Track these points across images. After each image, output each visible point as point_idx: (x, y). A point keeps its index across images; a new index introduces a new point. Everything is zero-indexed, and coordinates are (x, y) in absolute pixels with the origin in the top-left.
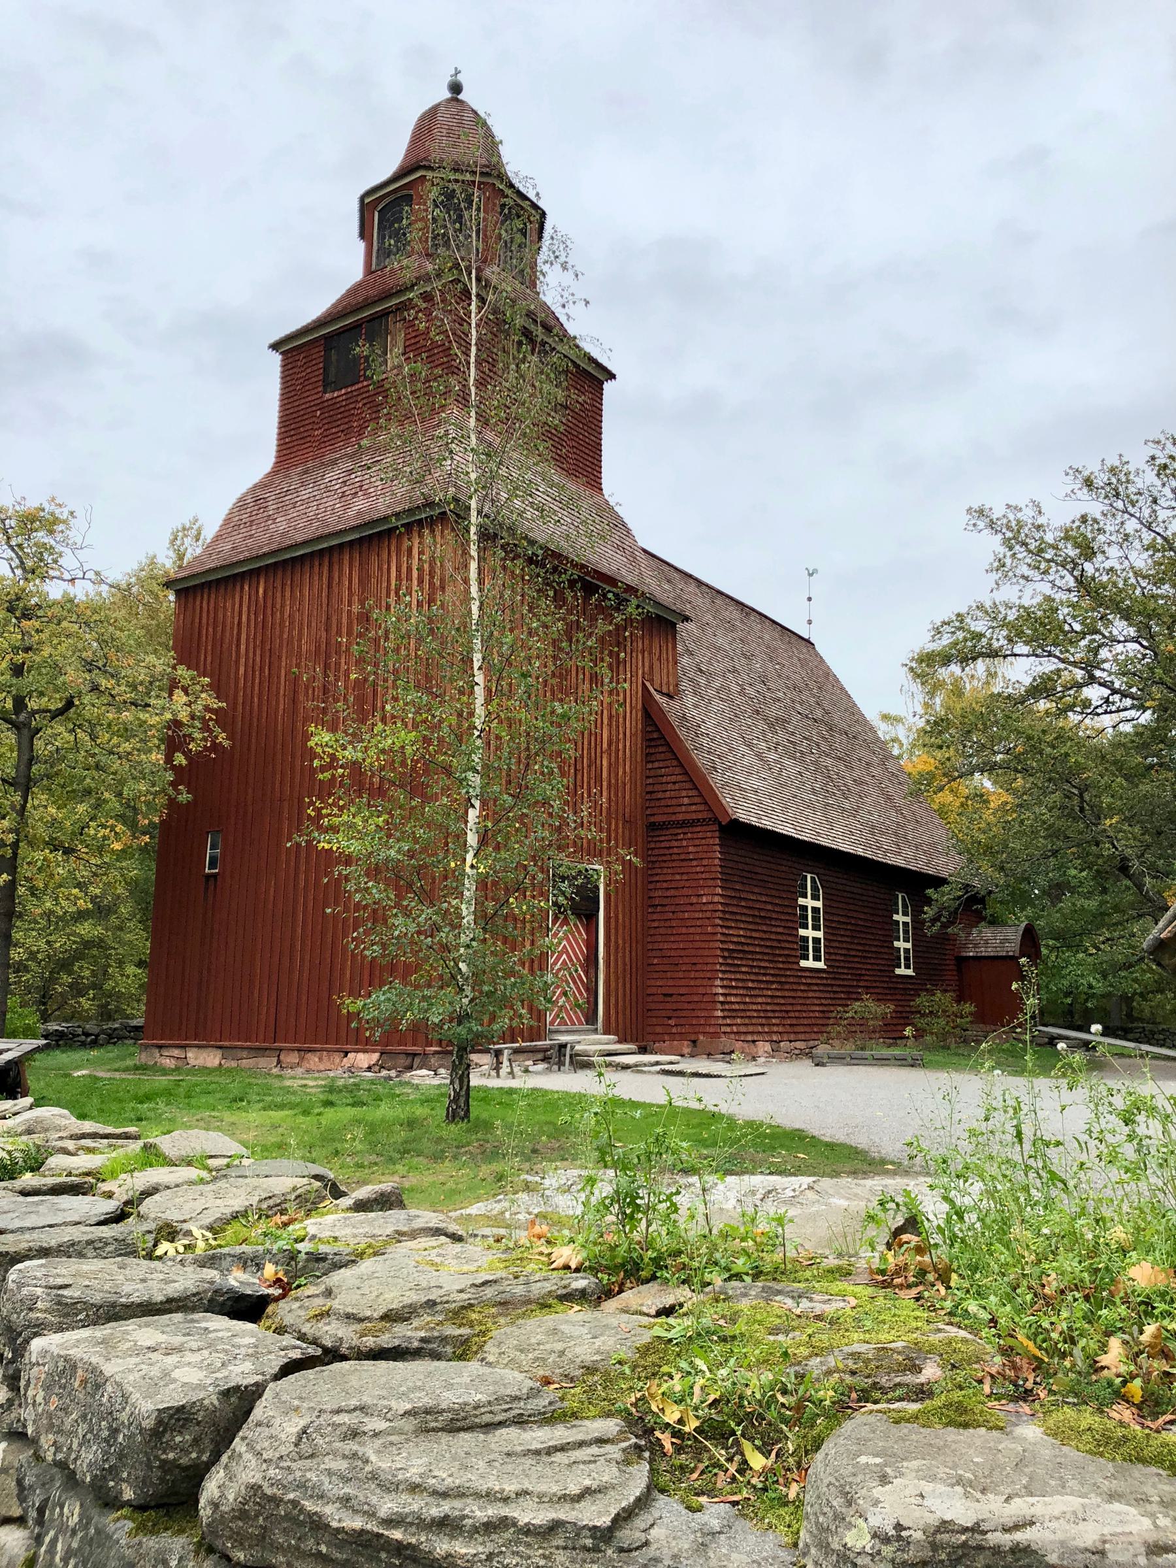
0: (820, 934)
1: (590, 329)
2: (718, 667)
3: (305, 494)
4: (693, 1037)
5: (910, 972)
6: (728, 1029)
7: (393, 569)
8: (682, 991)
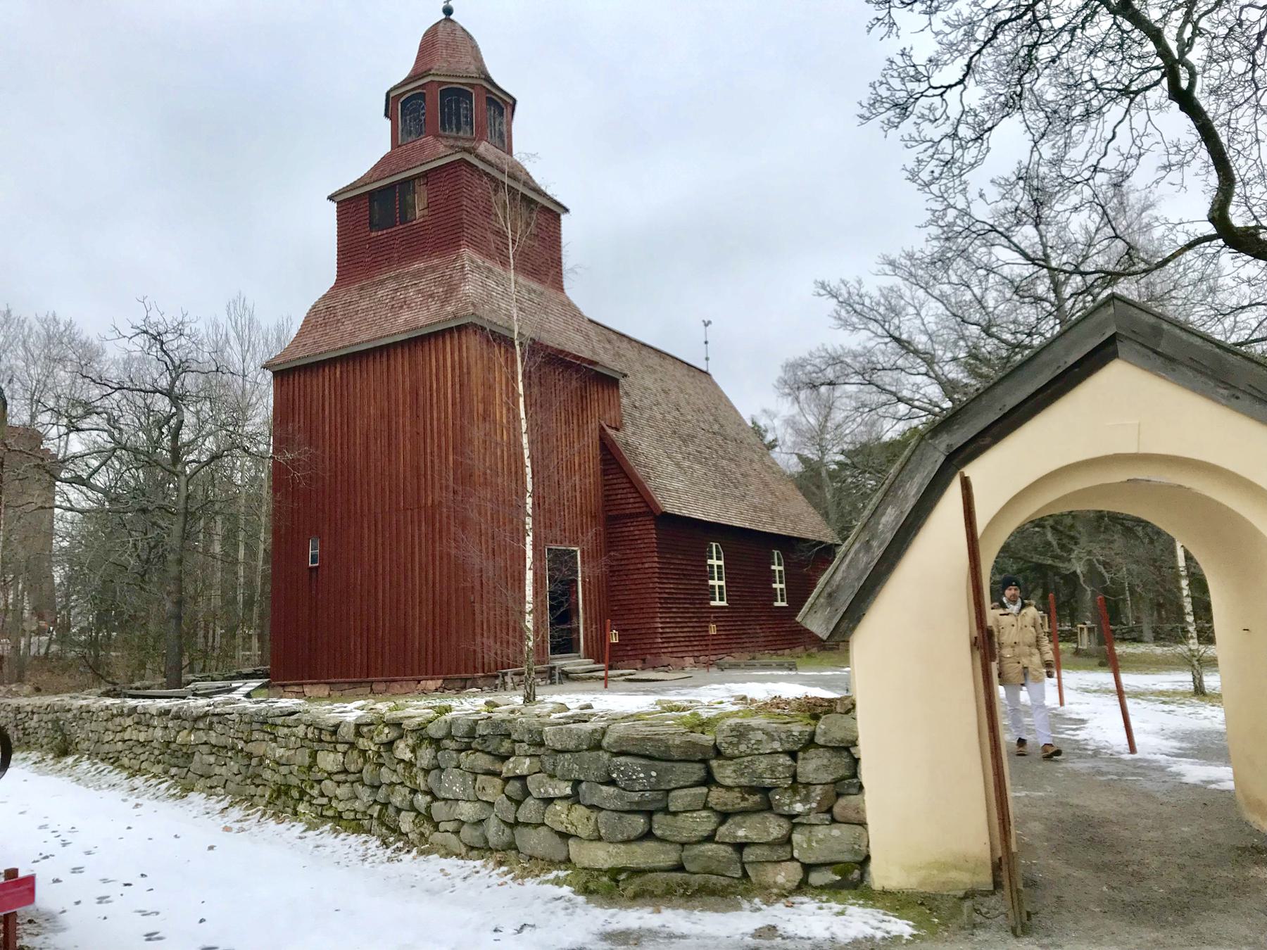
1: (550, 177)
2: (647, 402)
3: (364, 304)
5: (784, 604)
7: (434, 360)
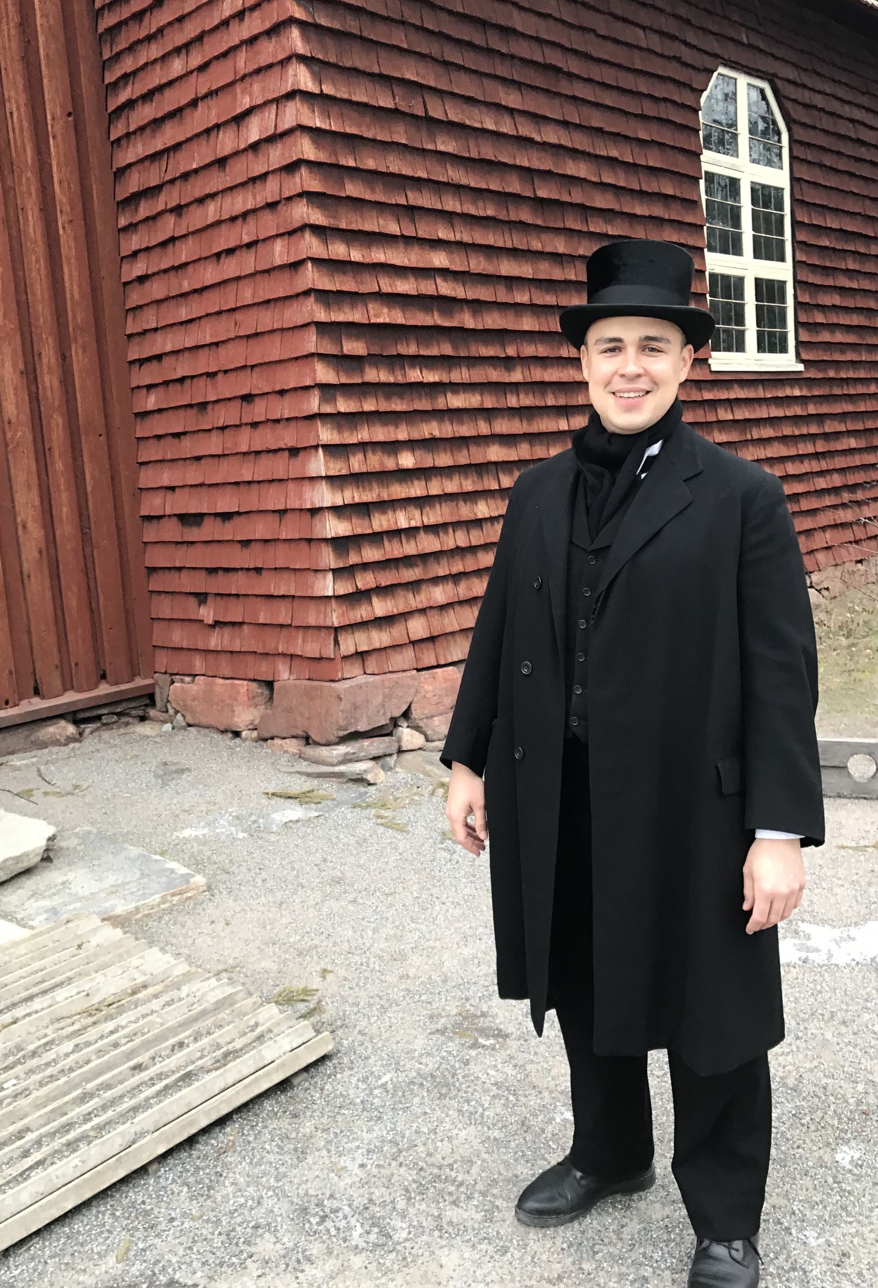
0: (781, 271)
4: (263, 670)
6: (379, 638)
8: (226, 502)
